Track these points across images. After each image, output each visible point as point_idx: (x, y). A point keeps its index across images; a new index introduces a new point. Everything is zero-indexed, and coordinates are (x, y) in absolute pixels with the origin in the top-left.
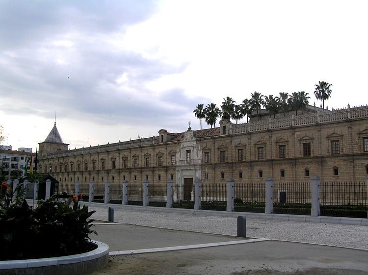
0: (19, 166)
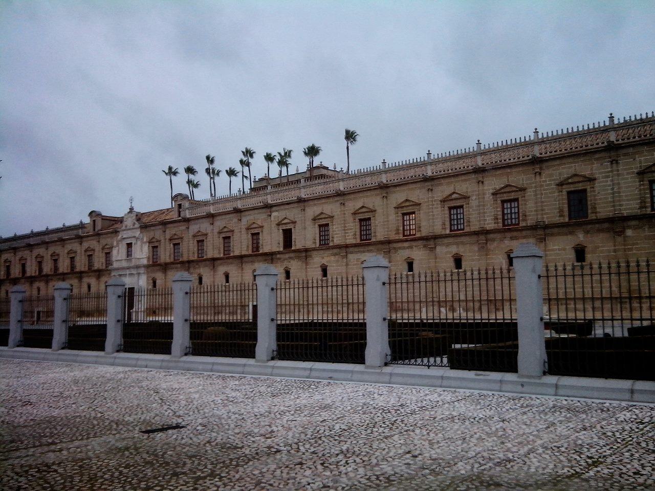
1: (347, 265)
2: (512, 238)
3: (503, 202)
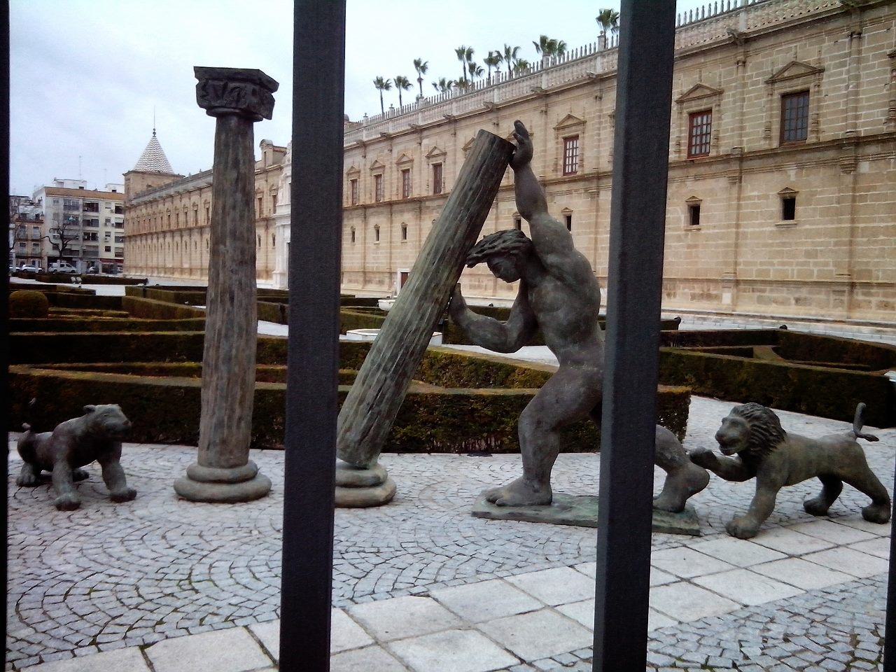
0: (102, 221)
2: (697, 178)
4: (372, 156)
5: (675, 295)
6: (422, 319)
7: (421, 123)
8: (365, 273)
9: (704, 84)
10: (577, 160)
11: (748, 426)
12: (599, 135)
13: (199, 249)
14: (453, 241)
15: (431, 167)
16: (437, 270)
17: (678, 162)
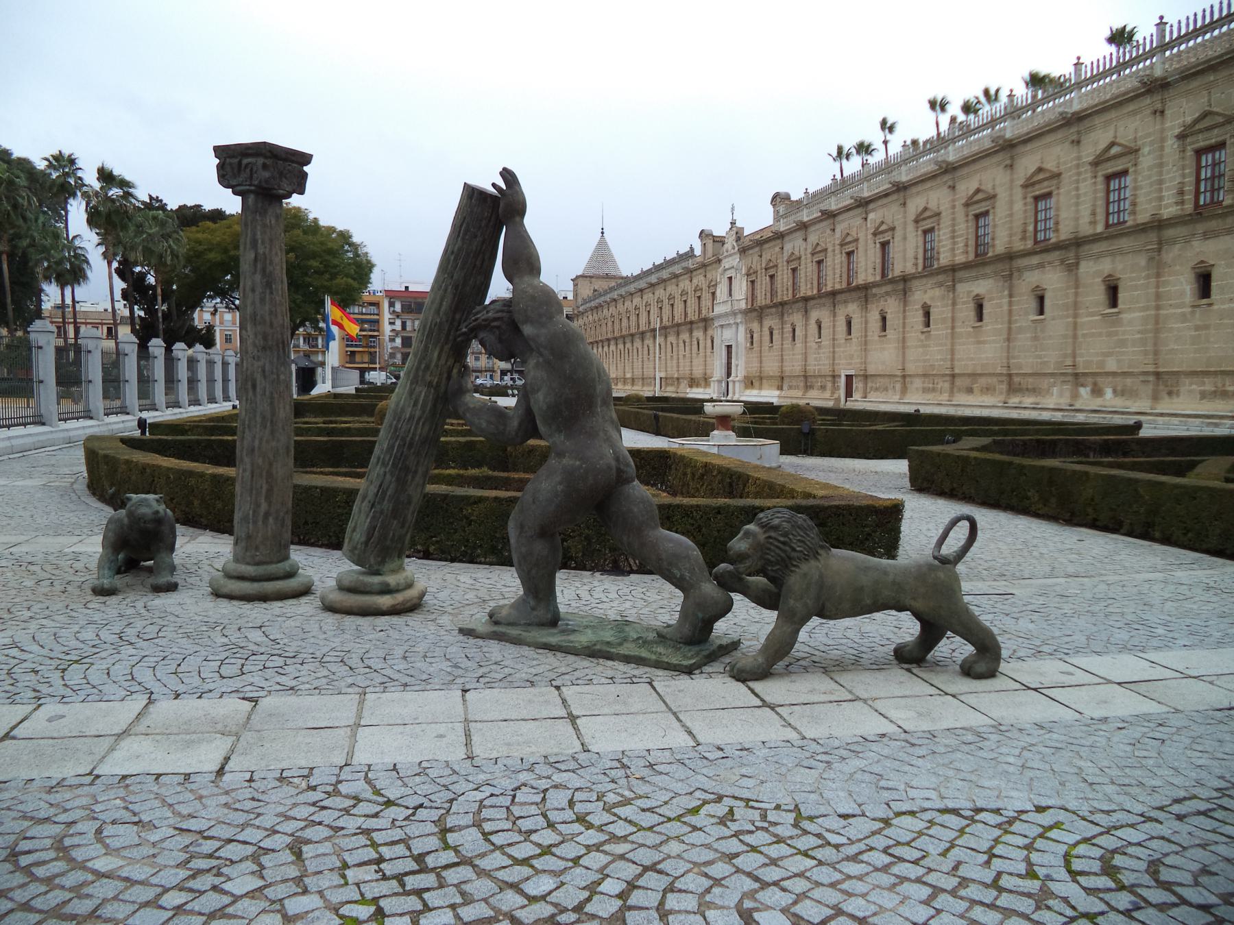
1: (954, 304)
2: (1206, 236)
3: (1199, 153)
4: (813, 238)
5: (1178, 394)
6: (415, 405)
7: (866, 194)
8: (806, 377)
9: (1215, 109)
10: (1051, 224)
11: (762, 537)
12: (1077, 189)
13: (640, 356)
14: (439, 314)
15: (878, 245)
16: (426, 347)
17: (1181, 216)
